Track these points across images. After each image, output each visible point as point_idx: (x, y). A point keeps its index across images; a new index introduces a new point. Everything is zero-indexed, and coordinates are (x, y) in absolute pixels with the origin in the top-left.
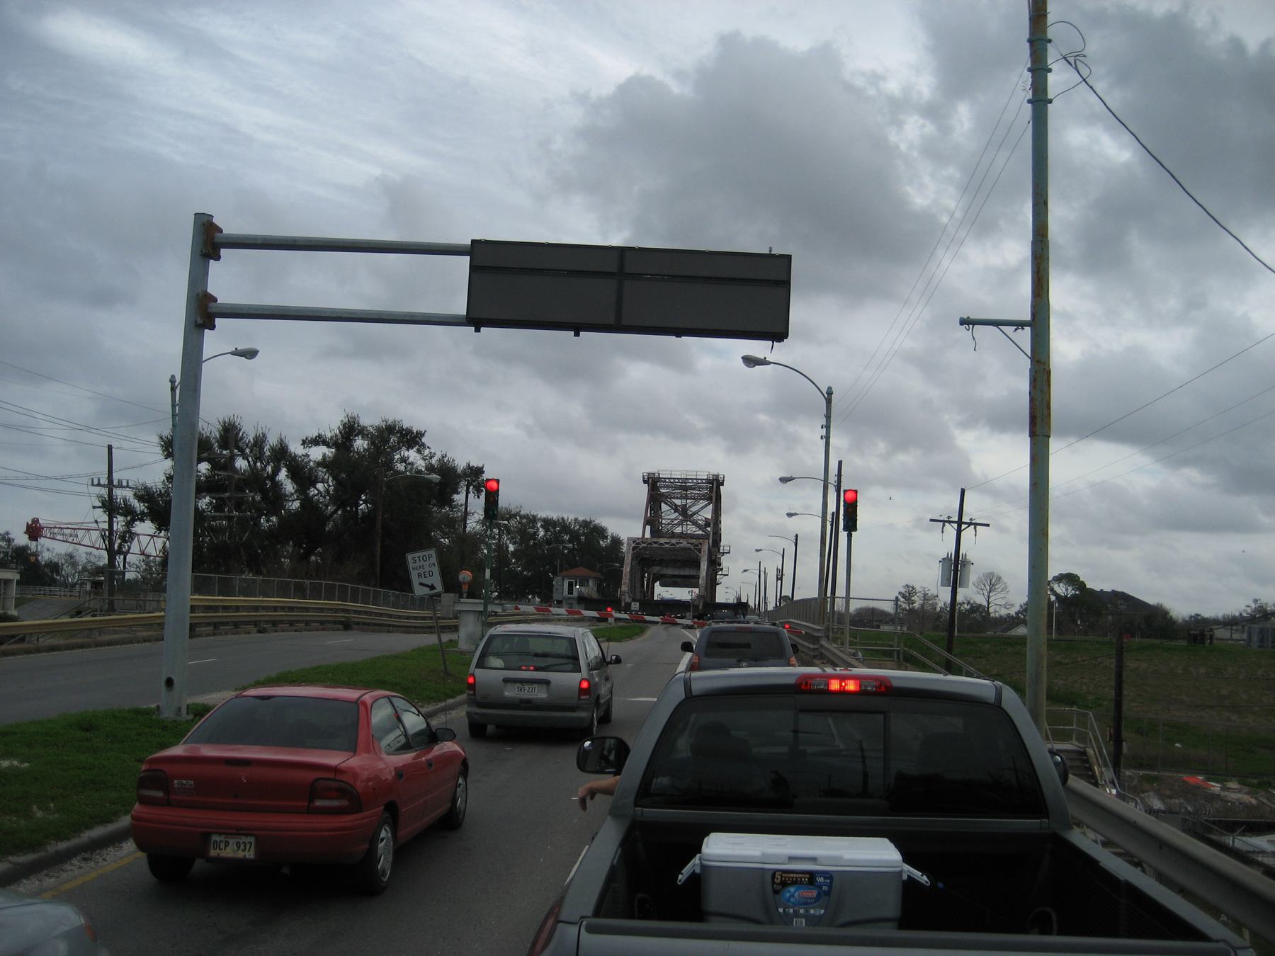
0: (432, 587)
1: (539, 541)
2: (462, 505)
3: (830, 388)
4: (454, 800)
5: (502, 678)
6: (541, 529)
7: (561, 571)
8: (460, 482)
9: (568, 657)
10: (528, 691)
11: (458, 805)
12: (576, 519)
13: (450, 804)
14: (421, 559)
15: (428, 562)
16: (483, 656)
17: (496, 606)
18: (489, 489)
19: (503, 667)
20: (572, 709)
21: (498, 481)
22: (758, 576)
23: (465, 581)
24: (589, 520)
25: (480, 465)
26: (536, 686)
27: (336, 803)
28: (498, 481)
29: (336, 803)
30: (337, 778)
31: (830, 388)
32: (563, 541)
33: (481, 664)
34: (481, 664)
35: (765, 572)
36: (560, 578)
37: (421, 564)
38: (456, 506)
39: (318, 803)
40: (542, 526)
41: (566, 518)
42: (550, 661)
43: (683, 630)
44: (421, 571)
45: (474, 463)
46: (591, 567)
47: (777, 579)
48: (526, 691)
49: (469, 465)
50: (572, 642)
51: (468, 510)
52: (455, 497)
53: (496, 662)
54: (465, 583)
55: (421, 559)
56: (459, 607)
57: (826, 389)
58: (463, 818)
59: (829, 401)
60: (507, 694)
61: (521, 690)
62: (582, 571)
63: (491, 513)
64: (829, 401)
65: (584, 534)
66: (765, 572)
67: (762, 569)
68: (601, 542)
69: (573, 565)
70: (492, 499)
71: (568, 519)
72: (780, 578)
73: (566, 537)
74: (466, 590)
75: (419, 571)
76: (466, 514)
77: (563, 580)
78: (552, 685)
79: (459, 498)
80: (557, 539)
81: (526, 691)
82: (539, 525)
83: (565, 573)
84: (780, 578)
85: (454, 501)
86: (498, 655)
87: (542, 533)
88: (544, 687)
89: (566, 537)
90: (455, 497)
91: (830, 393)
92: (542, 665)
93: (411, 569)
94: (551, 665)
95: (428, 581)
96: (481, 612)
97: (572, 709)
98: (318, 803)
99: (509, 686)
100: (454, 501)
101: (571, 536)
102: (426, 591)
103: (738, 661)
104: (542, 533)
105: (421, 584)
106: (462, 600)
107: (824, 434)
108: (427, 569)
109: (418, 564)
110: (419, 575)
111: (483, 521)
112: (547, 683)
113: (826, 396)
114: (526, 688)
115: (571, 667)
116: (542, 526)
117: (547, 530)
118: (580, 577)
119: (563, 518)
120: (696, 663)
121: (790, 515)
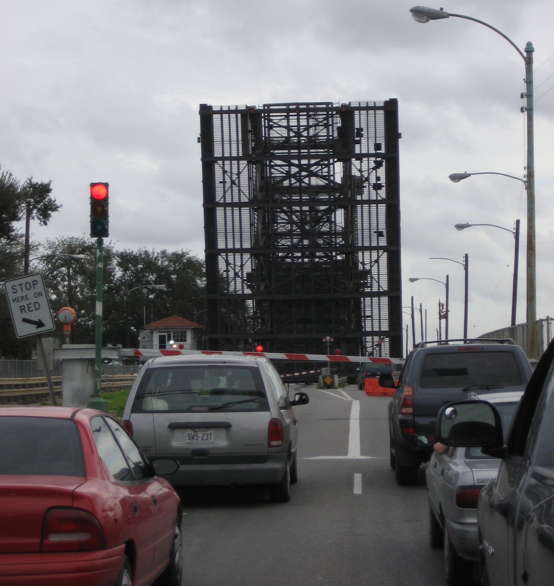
0: (40, 324)
1: (115, 284)
2: (22, 236)
3: (529, 45)
4: (172, 555)
5: (167, 424)
6: (117, 268)
7: (148, 323)
8: (20, 204)
9: (250, 393)
10: (202, 439)
11: (176, 563)
12: (164, 253)
13: (169, 559)
14: (23, 286)
15: (32, 291)
16: (140, 397)
17: (111, 351)
18: (96, 197)
19: (167, 409)
20: (262, 459)
21: (106, 185)
22: (410, 316)
23: (68, 321)
24: (180, 253)
25: (46, 182)
26: (211, 431)
27: (74, 538)
28: (106, 185)
29: (74, 538)
30: (74, 505)
31: (529, 45)
32: (148, 282)
33: (137, 408)
34: (137, 408)
35: (421, 310)
36: (147, 332)
37: (23, 294)
38: (14, 238)
39: (54, 538)
40: (119, 264)
41: (150, 250)
42: (226, 399)
43: (320, 390)
44: (25, 303)
45: (37, 180)
46: (186, 314)
47: (441, 317)
48: (200, 439)
49: (30, 180)
50: (255, 372)
51: (30, 242)
52: (15, 225)
53: (160, 404)
54: (66, 324)
55: (23, 286)
56: (61, 356)
57: (525, 46)
58: (181, 578)
59: (529, 61)
60: (175, 444)
61: (193, 438)
62: (175, 321)
63: (99, 227)
64: (529, 61)
65: (175, 272)
66: (421, 310)
67: (416, 306)
68: (198, 281)
69: (160, 315)
70: (99, 209)
71: (153, 253)
72: (443, 315)
73: (152, 277)
74: (69, 333)
75: (21, 303)
76: (27, 248)
77: (152, 333)
78: (234, 428)
79: (18, 226)
80: (139, 277)
81: (200, 439)
82: (115, 262)
83: (153, 325)
84: (443, 315)
85: (13, 230)
86: (161, 395)
87: (118, 273)
88: (223, 432)
89: (152, 277)
90: (15, 225)
91: (530, 50)
92: (220, 404)
93: (11, 301)
94: (231, 403)
95: (34, 316)
96: (91, 362)
97: (262, 459)
98: (54, 538)
99: (178, 433)
100: (13, 230)
101: (159, 276)
102: (32, 330)
103: (464, 390)
104: (118, 273)
105: (25, 320)
106: (64, 346)
107: (525, 105)
108: (32, 300)
109: (19, 294)
110: (22, 309)
111: (83, 245)
112: (226, 426)
113: (525, 54)
114: (200, 434)
115: (254, 405)
116: (119, 264)
117: (125, 269)
118: (173, 328)
119: (146, 253)
120: (408, 396)
121: (460, 227)
